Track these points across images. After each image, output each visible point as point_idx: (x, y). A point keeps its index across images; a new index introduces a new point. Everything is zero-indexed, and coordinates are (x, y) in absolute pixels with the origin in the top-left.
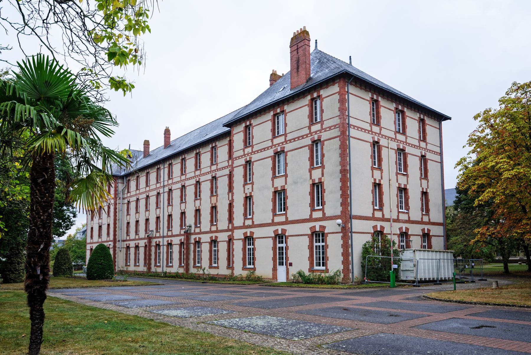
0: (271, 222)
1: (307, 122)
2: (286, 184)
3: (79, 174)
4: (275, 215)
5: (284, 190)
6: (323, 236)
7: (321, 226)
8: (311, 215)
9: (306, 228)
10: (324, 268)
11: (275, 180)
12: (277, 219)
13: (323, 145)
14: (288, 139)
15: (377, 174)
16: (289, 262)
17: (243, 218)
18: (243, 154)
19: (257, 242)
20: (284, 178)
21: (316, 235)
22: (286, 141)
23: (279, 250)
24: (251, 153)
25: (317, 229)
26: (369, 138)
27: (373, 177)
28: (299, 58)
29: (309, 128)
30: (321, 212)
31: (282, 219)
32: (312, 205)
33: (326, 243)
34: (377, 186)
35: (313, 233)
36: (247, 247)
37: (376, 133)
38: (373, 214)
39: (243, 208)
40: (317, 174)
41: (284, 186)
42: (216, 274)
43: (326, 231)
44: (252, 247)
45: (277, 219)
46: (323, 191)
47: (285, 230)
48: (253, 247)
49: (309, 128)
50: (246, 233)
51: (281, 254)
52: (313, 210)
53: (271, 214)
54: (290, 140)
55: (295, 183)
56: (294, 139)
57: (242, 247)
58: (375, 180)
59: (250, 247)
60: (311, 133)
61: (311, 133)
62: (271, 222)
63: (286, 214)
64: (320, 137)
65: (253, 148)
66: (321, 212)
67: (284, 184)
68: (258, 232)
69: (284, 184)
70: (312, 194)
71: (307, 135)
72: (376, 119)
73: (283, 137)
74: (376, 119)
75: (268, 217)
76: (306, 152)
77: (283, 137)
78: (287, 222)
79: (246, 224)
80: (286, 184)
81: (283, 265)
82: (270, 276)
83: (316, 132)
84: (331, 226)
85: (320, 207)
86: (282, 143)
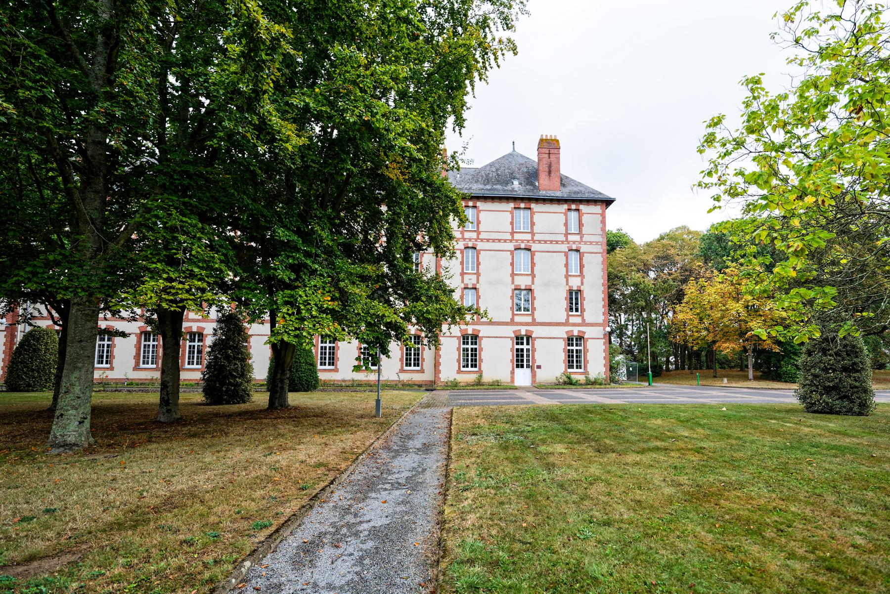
0: (509, 320)
2: (582, 284)
3: (97, 106)
5: (579, 291)
7: (579, 331)
8: (567, 319)
10: (108, 366)
12: (572, 320)
16: (536, 365)
19: (537, 343)
23: (464, 350)
28: (551, 163)
31: (578, 320)
33: (533, 346)
42: (150, 378)
46: (583, 299)
47: (584, 333)
55: (547, 285)
56: (488, 240)
62: (509, 320)
75: (562, 316)
78: (534, 323)
81: (522, 366)
82: (509, 380)
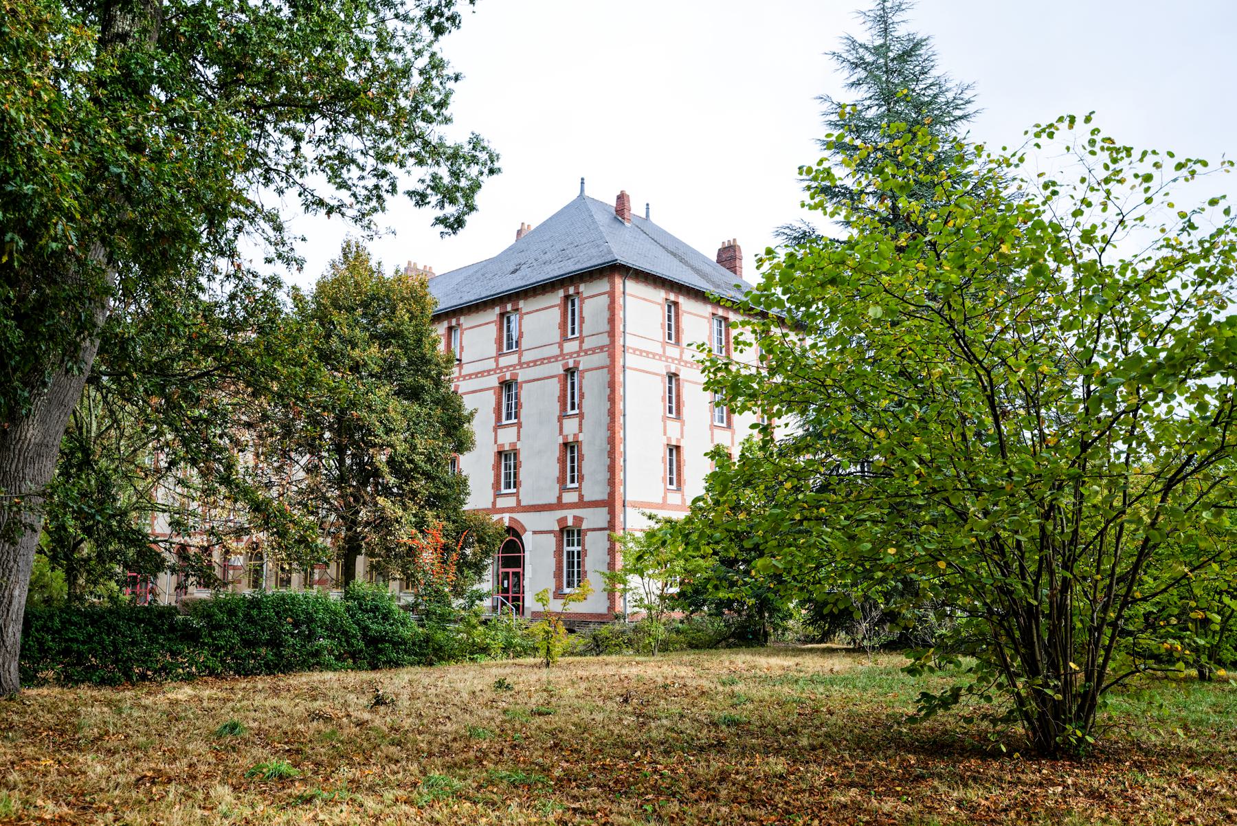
1: (556, 335)
2: (581, 431)
4: (497, 495)
6: (579, 535)
9: (549, 521)
11: (500, 431)
13: (582, 378)
14: (585, 346)
15: (673, 427)
17: (491, 492)
18: (577, 349)
20: (577, 420)
21: (568, 532)
22: (520, 364)
24: (578, 353)
25: (570, 523)
26: (661, 368)
27: (665, 434)
29: (561, 346)
30: (514, 499)
31: (511, 502)
32: (562, 480)
34: (674, 450)
35: (562, 530)
36: (566, 549)
37: (673, 359)
38: (665, 498)
39: (492, 473)
40: (571, 426)
41: (515, 444)
43: (584, 527)
44: (576, 548)
45: (502, 502)
48: (580, 548)
49: (561, 346)
50: (565, 519)
51: (570, 564)
52: (563, 489)
53: (491, 493)
54: (528, 363)
56: (535, 362)
57: (554, 548)
58: (669, 439)
59: (571, 549)
60: (562, 354)
61: (562, 354)
63: (517, 494)
64: (577, 363)
65: (582, 342)
66: (514, 499)
67: (515, 440)
68: (528, 521)
69: (515, 440)
70: (562, 461)
71: (556, 358)
72: (673, 332)
73: (577, 343)
74: (673, 332)
76: (554, 387)
77: (577, 343)
79: (498, 506)
80: (581, 431)
83: (571, 355)
84: (594, 518)
85: (576, 485)
86: (514, 366)
